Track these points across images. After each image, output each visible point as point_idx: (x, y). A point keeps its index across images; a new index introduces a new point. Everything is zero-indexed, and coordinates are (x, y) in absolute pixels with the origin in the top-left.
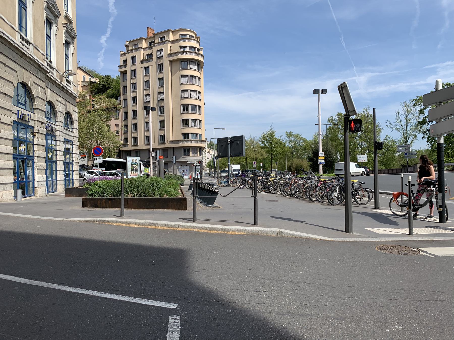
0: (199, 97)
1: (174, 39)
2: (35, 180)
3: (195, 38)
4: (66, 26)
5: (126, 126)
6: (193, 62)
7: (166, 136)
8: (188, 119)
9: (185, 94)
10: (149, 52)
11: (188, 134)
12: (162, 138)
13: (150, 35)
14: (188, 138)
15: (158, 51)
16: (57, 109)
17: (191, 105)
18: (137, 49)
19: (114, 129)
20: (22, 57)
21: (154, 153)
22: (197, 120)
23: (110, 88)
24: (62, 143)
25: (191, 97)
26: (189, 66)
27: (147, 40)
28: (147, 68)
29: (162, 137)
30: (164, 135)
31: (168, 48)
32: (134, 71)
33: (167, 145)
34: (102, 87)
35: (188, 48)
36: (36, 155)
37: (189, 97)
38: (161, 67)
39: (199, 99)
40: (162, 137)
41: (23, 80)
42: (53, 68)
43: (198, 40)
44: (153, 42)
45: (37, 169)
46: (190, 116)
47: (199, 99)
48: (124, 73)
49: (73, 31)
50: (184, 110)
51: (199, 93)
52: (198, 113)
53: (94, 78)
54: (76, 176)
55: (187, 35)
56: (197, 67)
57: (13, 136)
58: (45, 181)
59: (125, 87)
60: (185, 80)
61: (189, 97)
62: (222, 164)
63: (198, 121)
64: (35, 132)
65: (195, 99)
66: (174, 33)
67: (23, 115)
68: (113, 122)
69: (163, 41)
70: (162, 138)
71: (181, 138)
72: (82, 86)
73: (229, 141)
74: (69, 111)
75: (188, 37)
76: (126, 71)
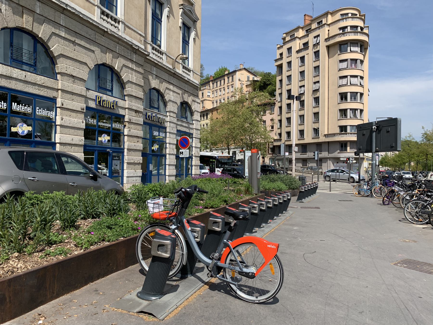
0: (360, 83)
1: (333, 21)
2: (124, 176)
3: (358, 16)
4: (182, 7)
5: (280, 121)
6: (354, 43)
7: (320, 129)
8: (347, 109)
9: (344, 81)
10: (304, 41)
11: (345, 127)
12: (316, 131)
13: (308, 22)
14: (346, 131)
15: (315, 37)
16: (167, 98)
17: (350, 92)
18: (293, 39)
19: (269, 123)
20: (103, 36)
21: (297, 148)
22: (357, 109)
23: (270, 84)
24: (175, 136)
25: (350, 84)
26: (349, 48)
27: (304, 29)
28: (302, 59)
29: (316, 131)
30: (318, 128)
31: (324, 32)
32: (289, 63)
33: (322, 139)
34: (263, 84)
35: (349, 28)
36: (126, 147)
37: (349, 84)
38: (317, 54)
39: (361, 85)
40: (316, 131)
41: (104, 62)
42: (162, 53)
43: (363, 18)
44: (310, 29)
45: (127, 163)
46: (349, 105)
47: (361, 85)
48: (280, 67)
49: (194, 13)
50: (342, 99)
51: (362, 78)
52: (359, 101)
53: (258, 77)
54: (195, 171)
55: (348, 14)
56: (359, 48)
57: (84, 124)
58: (140, 176)
59: (281, 81)
60: (344, 65)
61: (349, 84)
62: (396, 161)
63: (359, 110)
64: (125, 122)
65: (356, 85)
66: (333, 14)
67: (104, 101)
68: (267, 117)
69: (321, 25)
70: (316, 131)
71: (338, 130)
72: (246, 86)
73: (373, 127)
74: (186, 100)
75: (350, 15)
76: (282, 64)
